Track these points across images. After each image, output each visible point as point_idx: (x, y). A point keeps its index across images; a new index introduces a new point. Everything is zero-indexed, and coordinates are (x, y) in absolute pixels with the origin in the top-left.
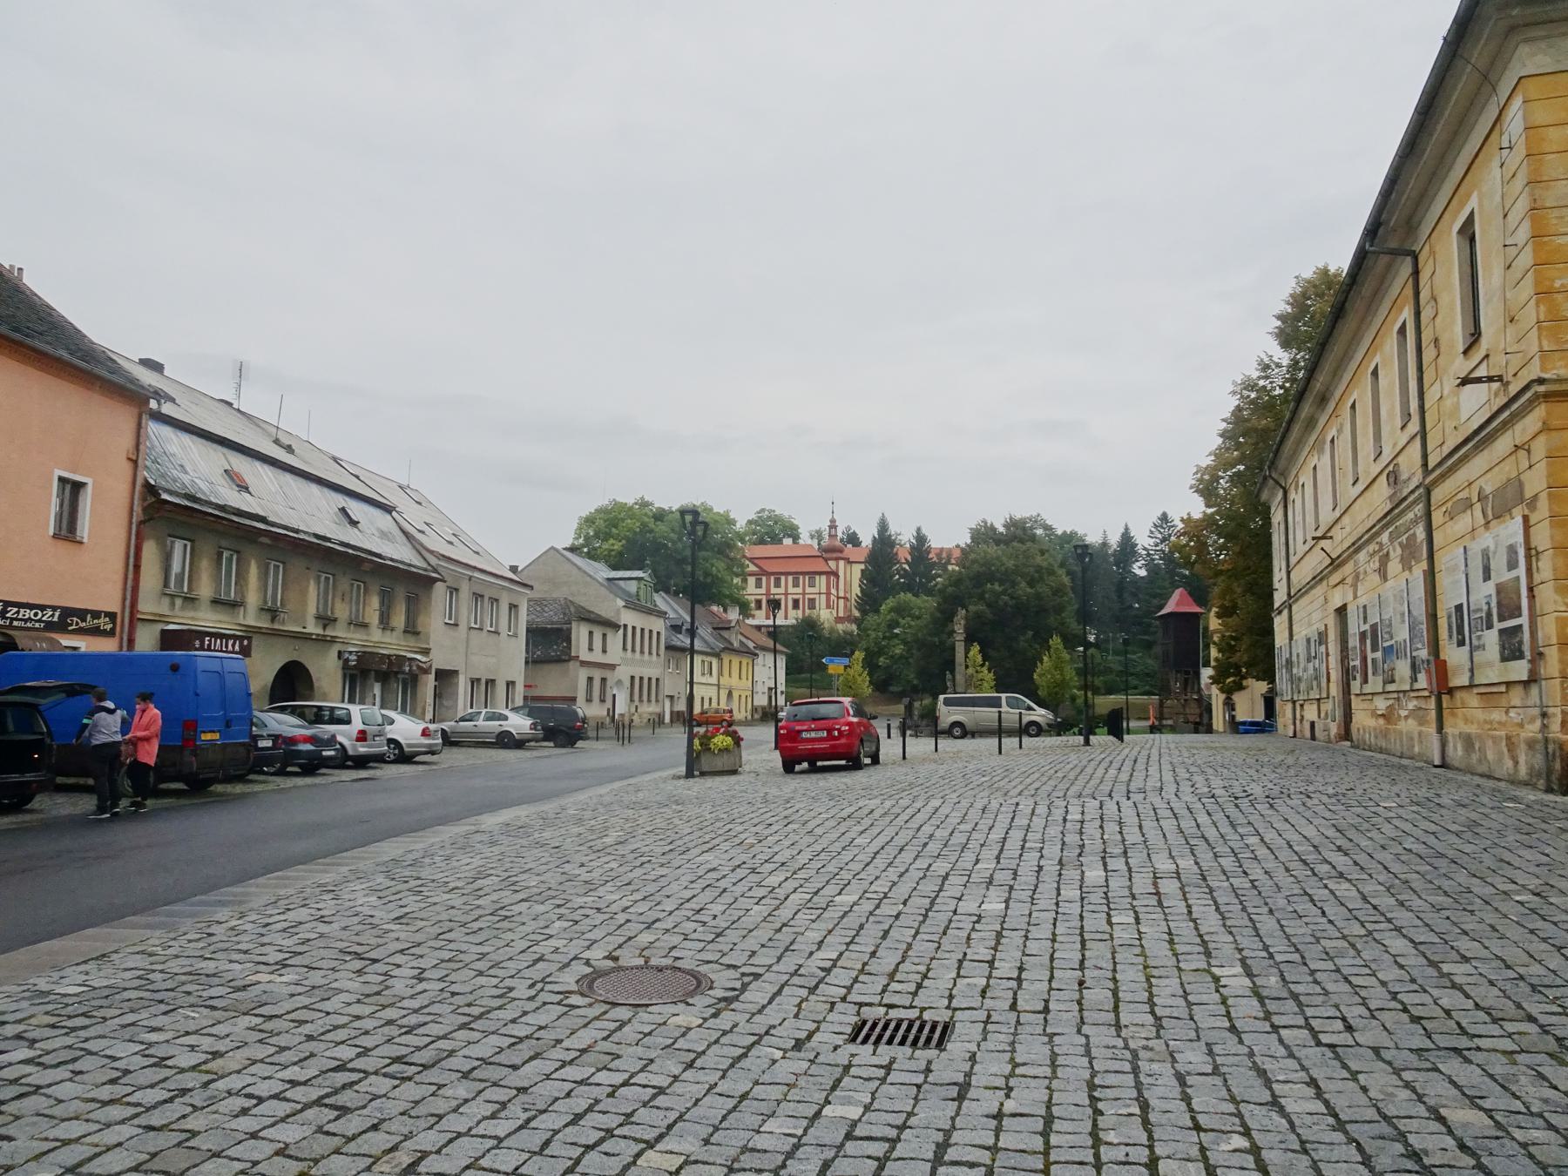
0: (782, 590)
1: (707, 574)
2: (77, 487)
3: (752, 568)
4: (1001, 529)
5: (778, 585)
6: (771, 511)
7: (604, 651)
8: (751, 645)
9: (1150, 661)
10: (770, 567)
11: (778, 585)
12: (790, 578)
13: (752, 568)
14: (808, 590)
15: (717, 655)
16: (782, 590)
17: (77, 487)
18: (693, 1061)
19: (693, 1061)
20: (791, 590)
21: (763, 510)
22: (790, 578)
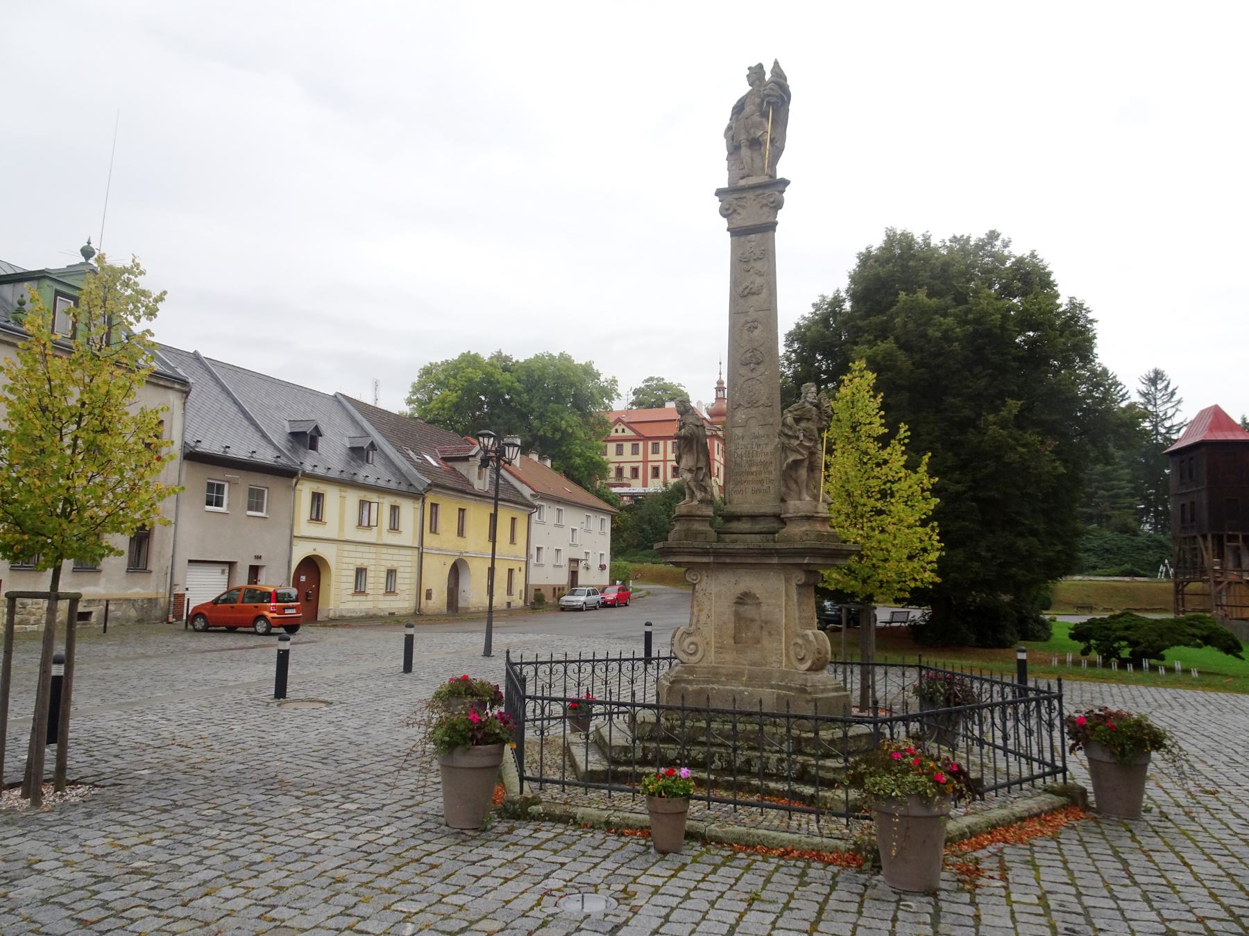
0: (660, 457)
1: (556, 429)
2: (436, 505)
3: (628, 433)
4: (406, 409)
5: (655, 451)
6: (659, 379)
7: (461, 533)
8: (527, 492)
9: (1108, 534)
10: (646, 431)
11: (655, 451)
12: (650, 443)
13: (628, 433)
14: (651, 457)
15: (415, 495)
16: (660, 457)
17: (436, 505)
18: (668, 915)
19: (668, 915)
20: (651, 457)
21: (651, 379)
22: (650, 443)
